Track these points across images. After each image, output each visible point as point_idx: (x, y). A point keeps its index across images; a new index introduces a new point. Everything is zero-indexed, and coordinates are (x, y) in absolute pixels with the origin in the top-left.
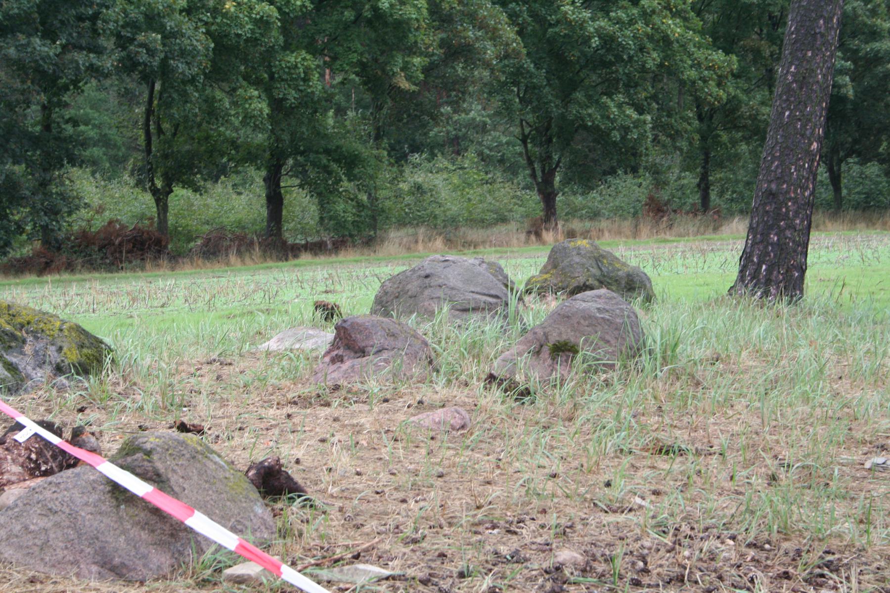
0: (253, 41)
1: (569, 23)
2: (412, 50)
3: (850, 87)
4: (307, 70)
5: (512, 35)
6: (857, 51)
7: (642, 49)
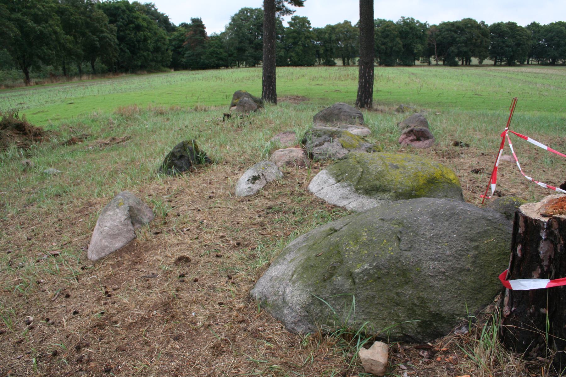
7: (50, 34)
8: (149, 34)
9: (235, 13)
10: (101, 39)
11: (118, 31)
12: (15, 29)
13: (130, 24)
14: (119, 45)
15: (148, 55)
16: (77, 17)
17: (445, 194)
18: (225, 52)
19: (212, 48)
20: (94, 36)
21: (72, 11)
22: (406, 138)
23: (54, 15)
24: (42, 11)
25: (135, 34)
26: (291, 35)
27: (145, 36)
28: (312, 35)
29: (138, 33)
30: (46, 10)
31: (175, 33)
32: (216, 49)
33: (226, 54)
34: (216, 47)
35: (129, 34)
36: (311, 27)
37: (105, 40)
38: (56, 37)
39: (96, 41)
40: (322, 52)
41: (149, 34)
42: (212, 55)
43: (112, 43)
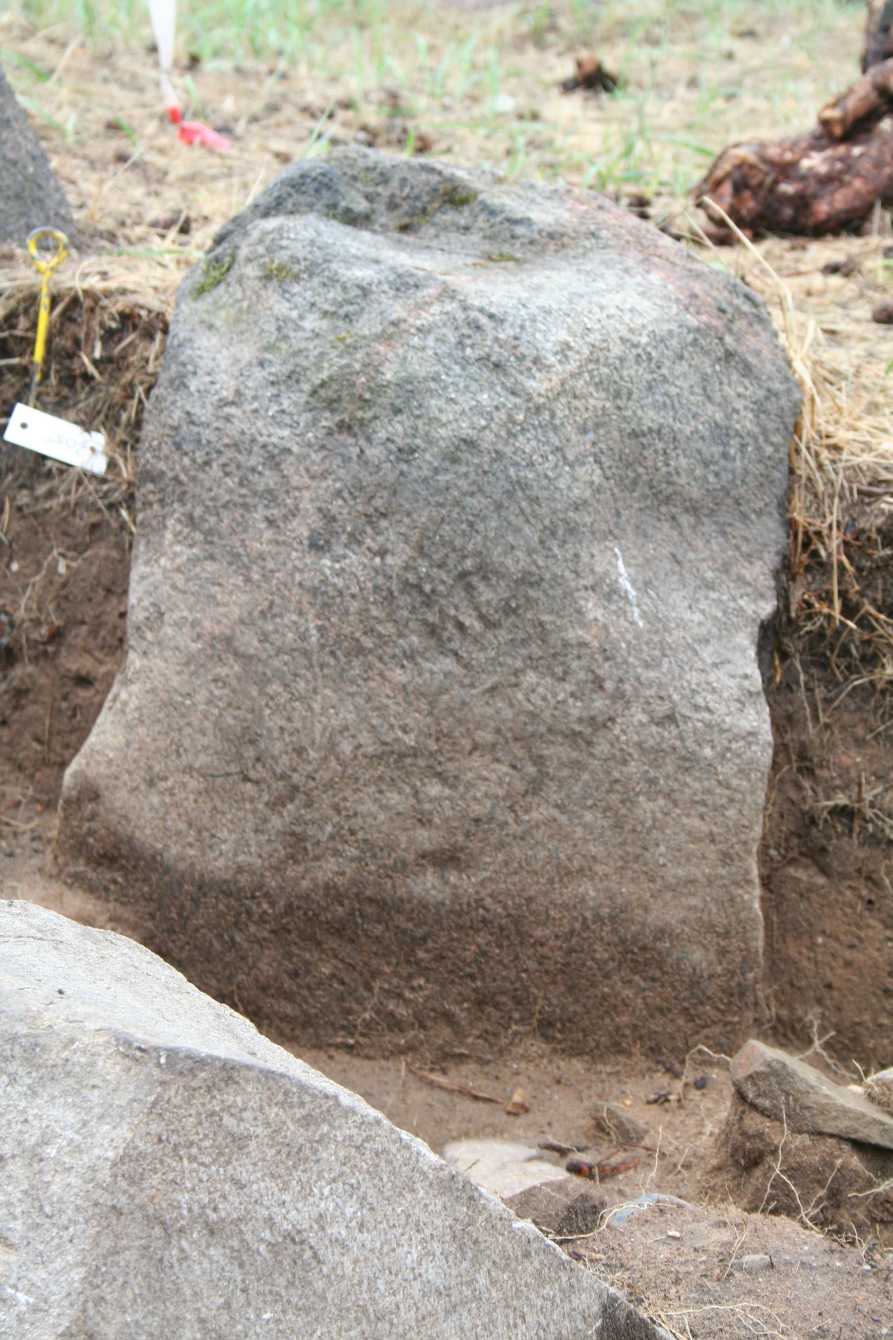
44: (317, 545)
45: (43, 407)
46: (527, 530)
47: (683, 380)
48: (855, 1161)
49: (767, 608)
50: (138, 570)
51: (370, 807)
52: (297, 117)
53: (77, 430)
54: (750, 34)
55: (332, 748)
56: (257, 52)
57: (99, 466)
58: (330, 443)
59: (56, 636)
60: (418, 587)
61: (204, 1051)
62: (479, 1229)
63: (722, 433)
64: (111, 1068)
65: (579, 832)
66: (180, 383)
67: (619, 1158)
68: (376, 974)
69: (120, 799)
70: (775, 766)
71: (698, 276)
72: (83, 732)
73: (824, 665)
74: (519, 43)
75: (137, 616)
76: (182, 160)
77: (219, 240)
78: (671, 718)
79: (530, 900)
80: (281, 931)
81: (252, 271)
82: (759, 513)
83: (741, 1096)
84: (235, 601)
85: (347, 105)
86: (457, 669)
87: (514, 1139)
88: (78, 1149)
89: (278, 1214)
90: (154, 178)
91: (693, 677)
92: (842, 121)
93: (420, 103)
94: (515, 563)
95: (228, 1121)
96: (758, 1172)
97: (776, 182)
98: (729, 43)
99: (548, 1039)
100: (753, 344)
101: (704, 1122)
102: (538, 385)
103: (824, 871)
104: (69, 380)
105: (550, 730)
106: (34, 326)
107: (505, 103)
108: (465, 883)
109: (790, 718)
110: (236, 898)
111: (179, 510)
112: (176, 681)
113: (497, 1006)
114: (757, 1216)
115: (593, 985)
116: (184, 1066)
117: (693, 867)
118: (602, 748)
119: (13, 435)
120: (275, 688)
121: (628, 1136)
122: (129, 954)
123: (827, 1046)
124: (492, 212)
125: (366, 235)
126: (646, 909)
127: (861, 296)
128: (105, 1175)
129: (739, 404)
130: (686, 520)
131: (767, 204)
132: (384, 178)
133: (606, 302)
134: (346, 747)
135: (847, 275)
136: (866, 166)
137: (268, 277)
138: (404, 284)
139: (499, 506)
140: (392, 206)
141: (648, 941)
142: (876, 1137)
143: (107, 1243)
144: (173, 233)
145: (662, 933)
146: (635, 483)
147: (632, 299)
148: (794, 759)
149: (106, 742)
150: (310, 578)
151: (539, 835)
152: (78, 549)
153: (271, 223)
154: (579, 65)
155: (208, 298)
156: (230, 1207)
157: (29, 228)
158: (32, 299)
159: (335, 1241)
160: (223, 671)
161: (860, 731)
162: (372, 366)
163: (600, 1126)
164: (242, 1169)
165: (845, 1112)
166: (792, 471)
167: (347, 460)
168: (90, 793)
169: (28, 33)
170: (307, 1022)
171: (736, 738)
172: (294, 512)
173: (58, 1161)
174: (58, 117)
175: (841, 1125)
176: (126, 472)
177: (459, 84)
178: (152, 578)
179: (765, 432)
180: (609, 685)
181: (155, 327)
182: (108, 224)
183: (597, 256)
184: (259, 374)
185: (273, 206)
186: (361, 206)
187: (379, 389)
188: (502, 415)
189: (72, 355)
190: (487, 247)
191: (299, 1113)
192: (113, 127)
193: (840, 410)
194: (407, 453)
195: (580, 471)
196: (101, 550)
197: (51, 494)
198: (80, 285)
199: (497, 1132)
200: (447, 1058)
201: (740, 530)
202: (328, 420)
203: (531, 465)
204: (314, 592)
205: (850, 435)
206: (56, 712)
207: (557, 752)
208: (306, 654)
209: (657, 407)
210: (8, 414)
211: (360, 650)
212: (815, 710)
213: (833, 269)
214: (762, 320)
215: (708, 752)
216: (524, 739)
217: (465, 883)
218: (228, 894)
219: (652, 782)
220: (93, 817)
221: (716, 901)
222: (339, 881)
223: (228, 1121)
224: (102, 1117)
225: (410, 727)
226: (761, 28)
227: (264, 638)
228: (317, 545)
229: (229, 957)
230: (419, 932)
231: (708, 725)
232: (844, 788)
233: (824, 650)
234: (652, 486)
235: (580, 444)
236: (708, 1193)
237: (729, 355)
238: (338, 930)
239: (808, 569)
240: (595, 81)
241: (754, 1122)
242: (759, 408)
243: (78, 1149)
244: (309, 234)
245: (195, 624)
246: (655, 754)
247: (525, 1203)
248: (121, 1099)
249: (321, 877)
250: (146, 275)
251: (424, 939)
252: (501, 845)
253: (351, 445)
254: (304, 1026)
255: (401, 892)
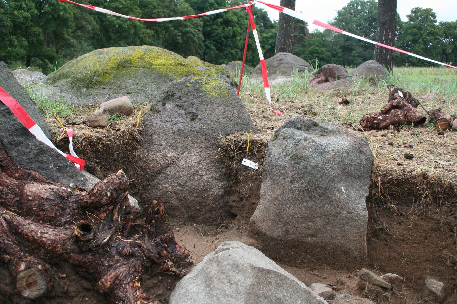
0: (23, 23)
1: (110, 21)
2: (68, 27)
3: (181, 39)
4: (39, 32)
5: (95, 24)
6: (182, 30)
7: (129, 28)
8: (239, 29)
9: (343, 6)
10: (184, 34)
11: (204, 27)
12: (94, 23)
13: (218, 18)
14: (204, 41)
15: (236, 52)
16: (159, 10)
17: (137, 81)
18: (328, 51)
19: (312, 47)
20: (177, 31)
21: (155, 5)
22: (314, 79)
23: (136, 9)
24: (123, 5)
25: (224, 29)
26: (409, 31)
27: (234, 32)
28: (437, 30)
29: (226, 29)
30: (128, 3)
31: (273, 30)
32: (317, 48)
33: (329, 54)
34: (317, 46)
35: (216, 29)
36: (436, 21)
37: (188, 35)
38: (135, 31)
39: (178, 36)
40: (449, 51)
41: (239, 29)
42: (312, 55)
43: (195, 39)
44: (291, 182)
45: (248, 159)
46: (326, 180)
47: (353, 156)
48: (380, 289)
49: (367, 194)
50: (262, 186)
51: (300, 226)
52: (294, 109)
53: (253, 162)
54: (373, 94)
55: (293, 216)
56: (289, 98)
57: (257, 168)
58: (294, 165)
59: (249, 196)
60: (308, 190)
61: (265, 268)
62: (311, 299)
63: (360, 165)
64: (249, 270)
65: (335, 231)
66: (269, 155)
67: (341, 287)
68: (301, 254)
69: (259, 224)
70: (369, 221)
71: (356, 138)
72: (253, 212)
73: (378, 204)
74: (333, 95)
75: (262, 194)
76: (274, 117)
77: (276, 132)
78: (351, 213)
79: (327, 243)
80: (285, 247)
81: (281, 137)
82: (366, 178)
83: (361, 278)
84: (278, 191)
85: (302, 107)
86: (314, 204)
87: (324, 283)
88: (244, 283)
89: (277, 295)
90: (268, 120)
91: (354, 206)
92: (385, 110)
93: (315, 106)
94: (324, 186)
95: (268, 279)
96: (364, 291)
97: (373, 121)
98: (369, 96)
99: (330, 266)
100: (365, 149)
101: (354, 283)
102: (328, 156)
103: (378, 239)
104: (253, 154)
105: (330, 214)
106: (247, 145)
107: (329, 106)
108: (316, 239)
109: (372, 213)
110: (277, 240)
111: (269, 176)
112: (268, 204)
113: (321, 260)
114: (362, 298)
115: (338, 257)
116: (261, 270)
117: (355, 238)
118: (339, 217)
119: (243, 163)
120: (284, 206)
121: (343, 284)
122: (255, 251)
123: (379, 269)
124: (321, 128)
125: (300, 131)
126: (347, 245)
127: (387, 140)
128: (248, 287)
129: (363, 160)
130: (353, 179)
131: (371, 124)
132: (304, 122)
133: (340, 142)
134: (296, 216)
135: (385, 137)
136: (389, 118)
137: (284, 138)
138: (306, 139)
139: (321, 177)
140: (305, 126)
141: (347, 250)
142: (384, 285)
143: (248, 298)
144: (270, 130)
145: (349, 249)
146: (345, 173)
147: (345, 142)
148: (372, 219)
149: (257, 214)
150: (290, 188)
151: (328, 232)
152: (253, 182)
153: (285, 129)
154: (343, 99)
155: (274, 142)
156: (269, 293)
157: (247, 129)
158: (247, 141)
159: (286, 300)
160: (276, 203)
161: (384, 215)
162: (301, 153)
163: (338, 282)
164: (271, 287)
165: (379, 281)
166: (372, 171)
167: (296, 168)
168: (254, 222)
169: (251, 96)
170: (289, 262)
171: (362, 216)
172: (288, 177)
173: (240, 285)
174: (254, 110)
175: (378, 283)
176: (261, 170)
177: (322, 103)
178: (264, 187)
179: (367, 164)
180: (340, 207)
181: (266, 146)
182: (260, 128)
183: (339, 135)
184: (282, 154)
185: (285, 126)
186: (300, 126)
187: (302, 157)
188: (322, 161)
189: (253, 150)
190: (320, 133)
191: (280, 278)
192: (263, 111)
193: (381, 160)
194: (306, 167)
195: (335, 171)
196: (257, 182)
197: (249, 173)
198: (254, 139)
199: (321, 282)
200: (312, 269)
201: (363, 181)
202: (293, 162)
203: (327, 170)
204: (291, 190)
205: (383, 165)
206: (249, 209)
207: (331, 218)
208: (289, 200)
209: (349, 160)
210: (242, 160)
211: (298, 200)
212: (376, 211)
213: (382, 136)
214: (367, 145)
215: (357, 218)
216: (326, 215)
217: (316, 239)
218: (276, 240)
219: (347, 223)
220: (254, 226)
221: (359, 244)
222: (295, 238)
223: (268, 279)
224: (248, 278)
225: (306, 213)
226: (375, 93)
227: (282, 198)
228: (291, 182)
229: (276, 251)
230: (308, 248)
231: (357, 214)
232: (381, 225)
233: (378, 202)
234: (347, 173)
235: (335, 166)
236: (355, 294)
237: (361, 151)
238: (294, 247)
239: (375, 187)
240: (346, 102)
241: (363, 282)
242: (366, 160)
243: (244, 283)
244: (291, 131)
245: (271, 195)
246: (348, 219)
247: (322, 295)
248: (251, 275)
249: (292, 238)
250: (266, 137)
251: (309, 249)
252: (322, 233)
253: (297, 166)
254: (289, 263)
255: (305, 241)
